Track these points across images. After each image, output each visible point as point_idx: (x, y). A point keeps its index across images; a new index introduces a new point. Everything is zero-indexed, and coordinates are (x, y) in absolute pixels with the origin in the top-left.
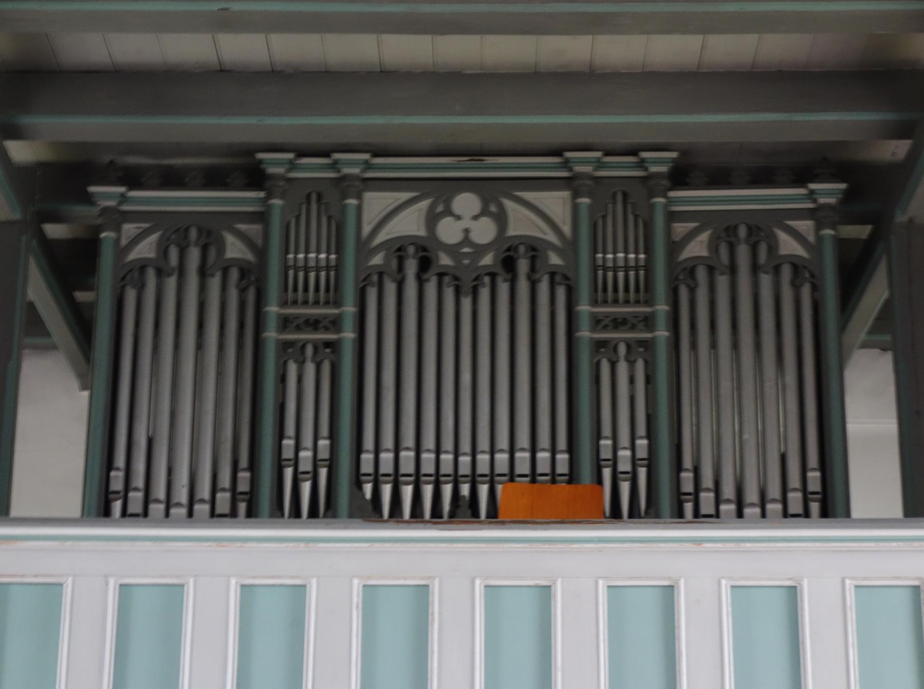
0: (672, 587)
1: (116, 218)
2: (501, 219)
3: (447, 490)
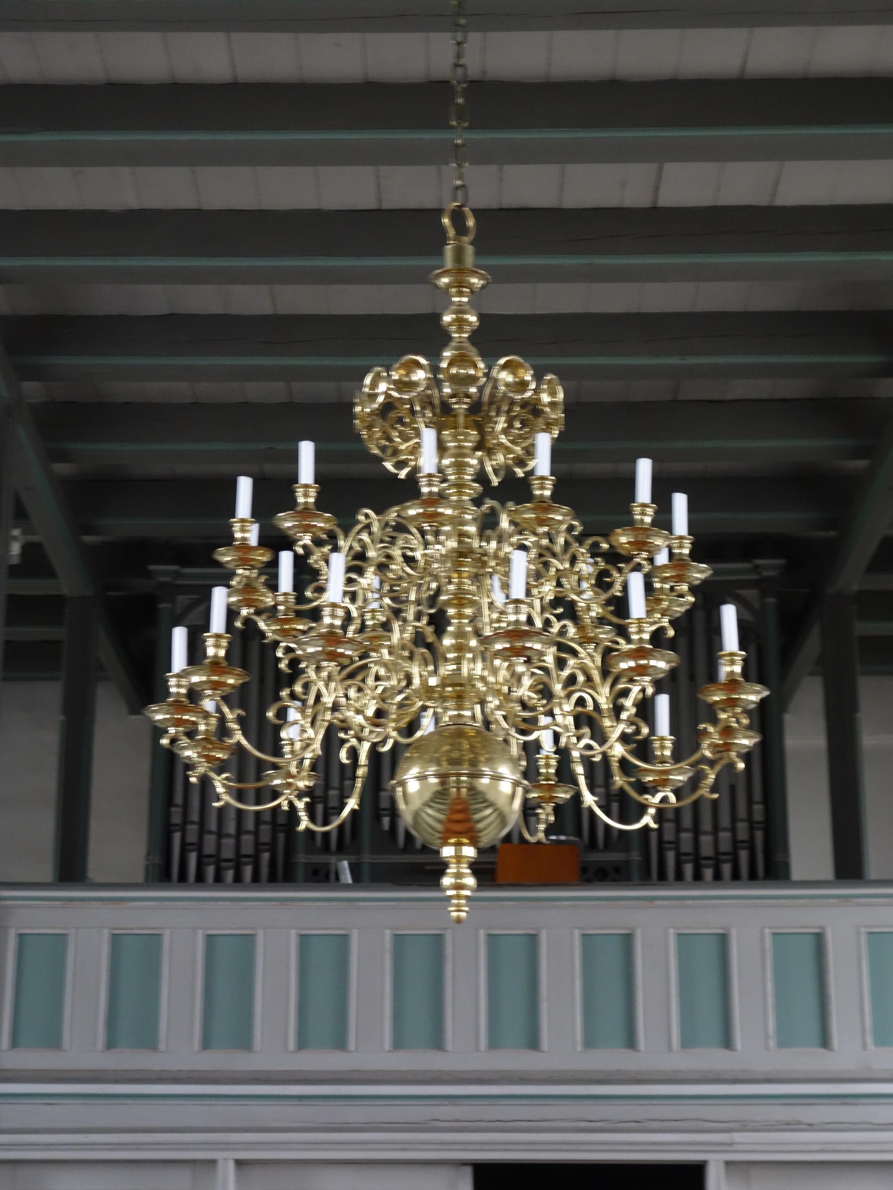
0: (630, 934)
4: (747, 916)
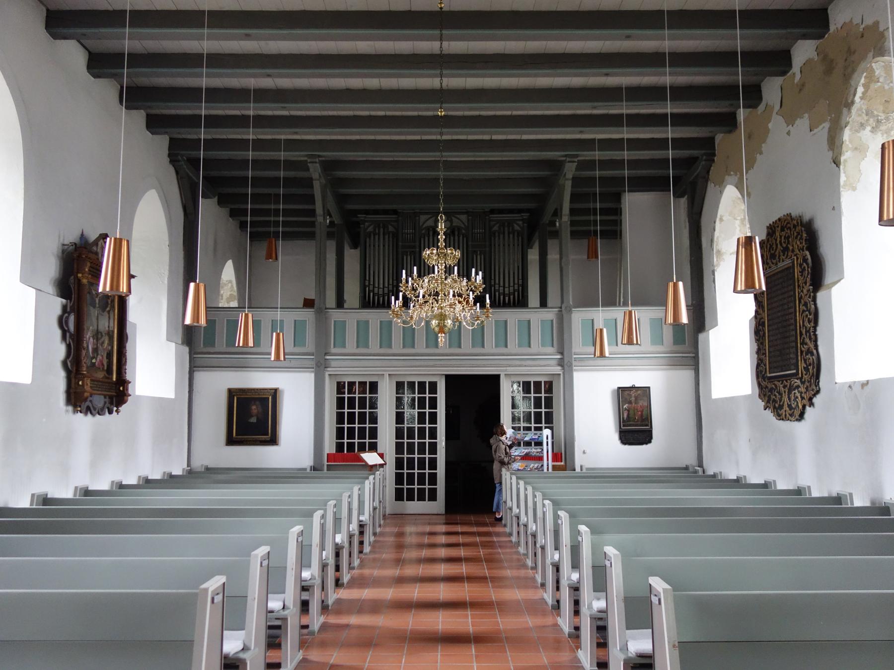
4: (513, 316)
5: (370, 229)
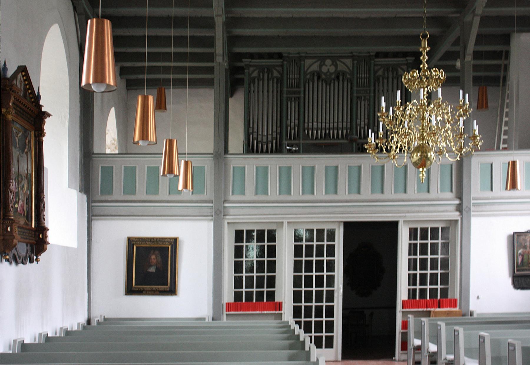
1: (249, 66)
2: (336, 66)
3: (324, 132)
5: (255, 74)
